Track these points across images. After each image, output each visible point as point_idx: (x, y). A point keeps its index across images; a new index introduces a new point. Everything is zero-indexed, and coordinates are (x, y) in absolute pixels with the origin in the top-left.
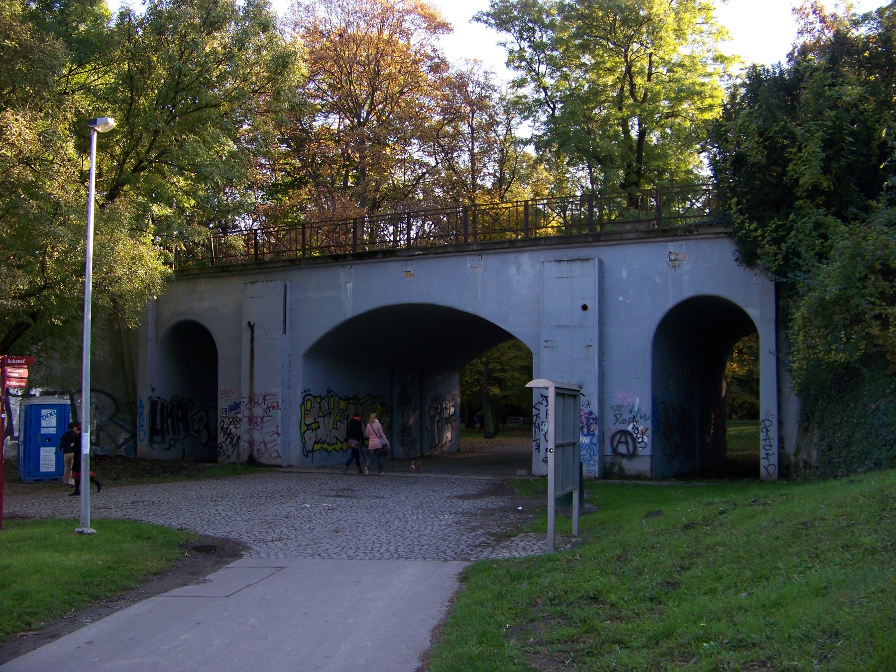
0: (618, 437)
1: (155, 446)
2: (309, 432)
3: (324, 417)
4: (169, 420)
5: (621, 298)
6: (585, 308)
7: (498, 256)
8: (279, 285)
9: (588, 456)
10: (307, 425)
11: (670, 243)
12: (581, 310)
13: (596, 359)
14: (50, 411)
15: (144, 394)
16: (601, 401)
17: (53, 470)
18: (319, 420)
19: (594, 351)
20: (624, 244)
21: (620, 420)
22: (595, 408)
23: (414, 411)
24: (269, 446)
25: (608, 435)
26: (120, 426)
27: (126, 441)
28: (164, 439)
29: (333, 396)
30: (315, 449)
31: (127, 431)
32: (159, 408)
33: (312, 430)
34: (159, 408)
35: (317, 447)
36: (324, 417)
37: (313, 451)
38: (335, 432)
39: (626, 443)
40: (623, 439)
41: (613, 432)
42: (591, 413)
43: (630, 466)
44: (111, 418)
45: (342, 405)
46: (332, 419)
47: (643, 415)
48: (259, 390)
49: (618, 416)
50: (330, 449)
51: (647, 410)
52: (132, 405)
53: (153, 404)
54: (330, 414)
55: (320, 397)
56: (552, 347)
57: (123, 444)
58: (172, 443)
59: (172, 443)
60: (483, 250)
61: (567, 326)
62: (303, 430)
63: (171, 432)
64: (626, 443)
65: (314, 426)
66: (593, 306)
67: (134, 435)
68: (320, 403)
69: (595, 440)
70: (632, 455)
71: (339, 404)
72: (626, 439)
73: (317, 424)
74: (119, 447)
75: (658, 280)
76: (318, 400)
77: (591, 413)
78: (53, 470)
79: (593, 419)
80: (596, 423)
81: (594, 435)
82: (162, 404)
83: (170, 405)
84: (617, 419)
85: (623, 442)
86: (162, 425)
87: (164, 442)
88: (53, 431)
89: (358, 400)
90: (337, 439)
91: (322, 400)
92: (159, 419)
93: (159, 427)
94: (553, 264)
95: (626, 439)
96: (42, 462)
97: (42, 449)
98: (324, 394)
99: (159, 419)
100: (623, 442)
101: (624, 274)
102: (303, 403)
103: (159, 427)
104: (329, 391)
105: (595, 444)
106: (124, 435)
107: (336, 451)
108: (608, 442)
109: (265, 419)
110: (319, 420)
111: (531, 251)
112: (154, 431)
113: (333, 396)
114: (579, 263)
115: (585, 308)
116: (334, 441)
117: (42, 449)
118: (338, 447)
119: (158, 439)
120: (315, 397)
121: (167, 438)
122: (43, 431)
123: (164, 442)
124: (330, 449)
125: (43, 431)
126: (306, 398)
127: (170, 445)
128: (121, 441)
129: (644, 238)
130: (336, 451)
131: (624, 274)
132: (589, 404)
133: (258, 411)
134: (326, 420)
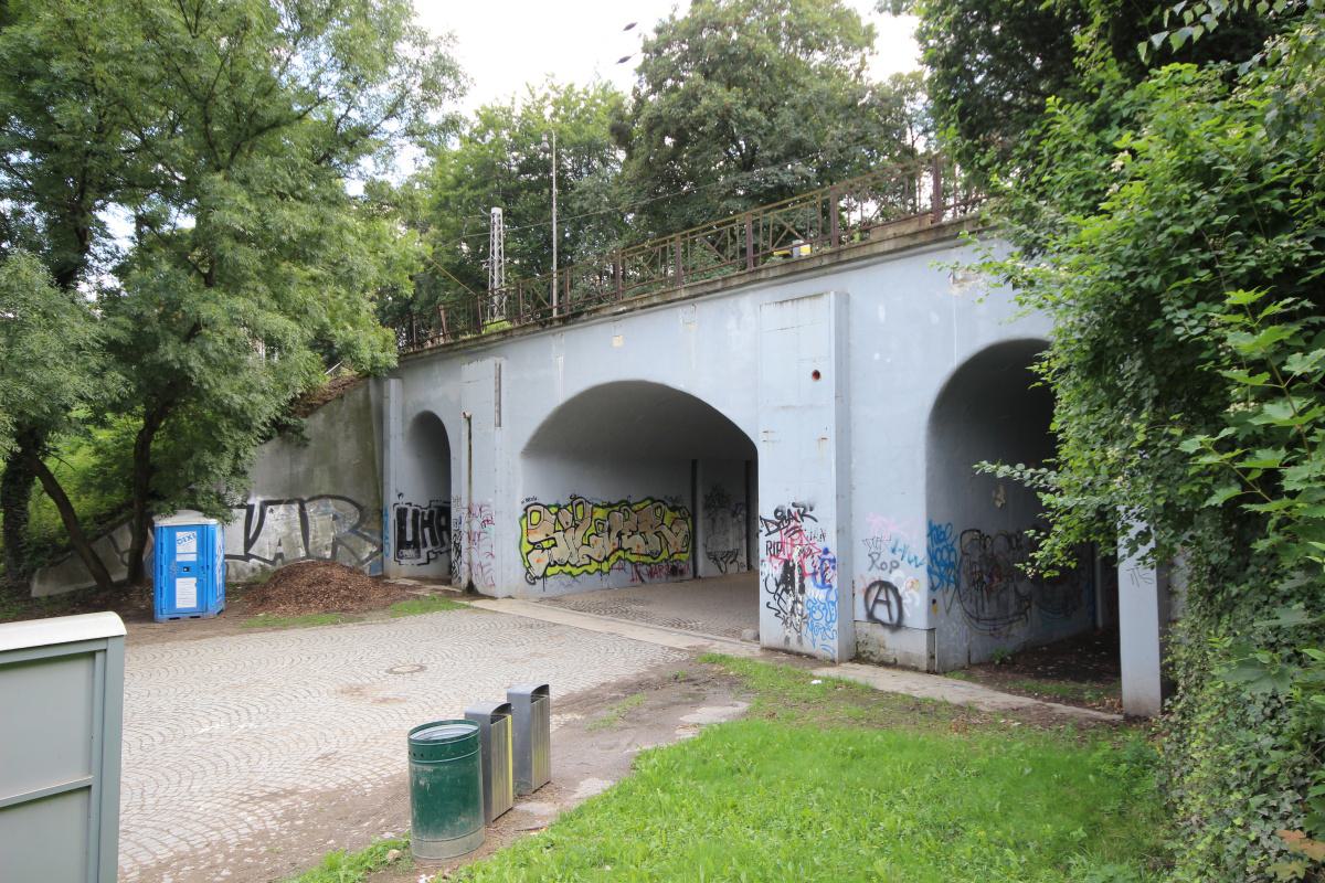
0: (874, 592)
1: (403, 561)
2: (537, 553)
3: (565, 531)
4: (427, 531)
5: (877, 356)
6: (817, 375)
7: (715, 303)
8: (824, 311)
9: (823, 622)
10: (534, 544)
11: (954, 251)
12: (818, 382)
13: (833, 461)
14: (190, 533)
15: (391, 499)
16: (843, 531)
17: (194, 605)
18: (556, 535)
19: (831, 446)
20: (875, 264)
21: (878, 563)
22: (831, 542)
23: (734, 514)
24: (485, 570)
25: (860, 587)
26: (365, 538)
27: (372, 555)
28: (419, 552)
29: (581, 503)
30: (548, 573)
31: (374, 544)
32: (409, 516)
33: (543, 549)
34: (409, 516)
35: (550, 571)
36: (565, 531)
37: (544, 575)
38: (586, 550)
39: (888, 603)
40: (882, 597)
41: (868, 582)
42: (826, 551)
43: (895, 644)
44: (354, 530)
45: (600, 513)
46: (580, 533)
47: (912, 557)
48: (476, 500)
49: (875, 556)
50: (575, 571)
51: (919, 545)
52: (381, 513)
53: (401, 513)
54: (576, 526)
55: (557, 506)
56: (773, 442)
57: (367, 560)
58: (432, 556)
59: (432, 556)
60: (695, 296)
61: (794, 407)
62: (524, 552)
63: (429, 543)
64: (888, 603)
65: (545, 544)
66: (828, 375)
67: (381, 549)
68: (556, 514)
69: (833, 597)
70: (897, 626)
71: (592, 513)
72: (887, 596)
73: (552, 542)
74: (363, 563)
75: (935, 318)
76: (554, 510)
77: (826, 551)
78: (194, 605)
79: (830, 560)
80: (834, 568)
81: (831, 587)
82: (416, 513)
83: (427, 512)
84: (874, 562)
85: (881, 602)
86: (415, 534)
87: (419, 557)
88: (193, 558)
89: (629, 505)
90: (590, 558)
91: (560, 509)
92: (409, 529)
93: (409, 538)
94: (772, 307)
95: (887, 596)
96: (178, 596)
97: (178, 580)
98: (564, 501)
99: (409, 529)
100: (881, 602)
101: (882, 314)
102: (525, 515)
103: (409, 538)
104: (574, 498)
105: (833, 604)
106: (371, 549)
107: (589, 573)
108: (860, 598)
109: (482, 536)
110: (556, 535)
111: (753, 290)
112: (402, 544)
113: (581, 503)
114: (807, 301)
115: (817, 375)
116: (587, 561)
117: (178, 580)
118: (591, 569)
119: (409, 552)
120: (547, 507)
121: (424, 552)
122: (179, 559)
123: (419, 557)
124: (575, 571)
125: (179, 559)
126: (530, 510)
127: (429, 560)
128: (366, 556)
129: (909, 247)
130: (589, 573)
131: (882, 314)
132: (823, 536)
133: (476, 526)
134: (570, 534)
